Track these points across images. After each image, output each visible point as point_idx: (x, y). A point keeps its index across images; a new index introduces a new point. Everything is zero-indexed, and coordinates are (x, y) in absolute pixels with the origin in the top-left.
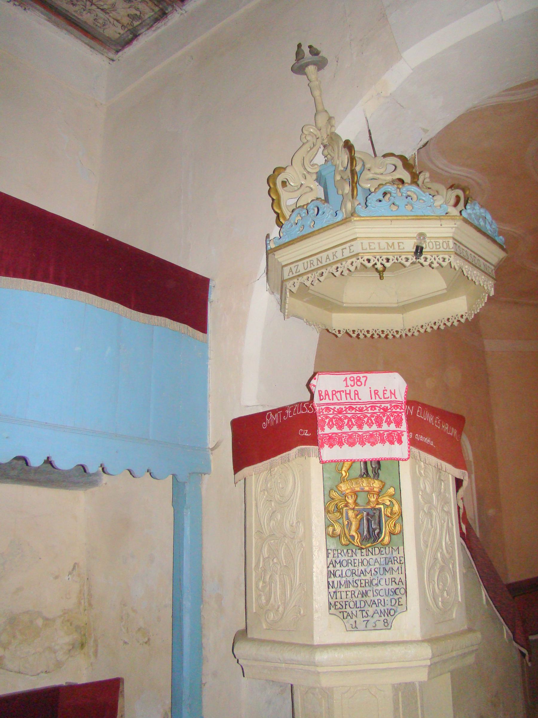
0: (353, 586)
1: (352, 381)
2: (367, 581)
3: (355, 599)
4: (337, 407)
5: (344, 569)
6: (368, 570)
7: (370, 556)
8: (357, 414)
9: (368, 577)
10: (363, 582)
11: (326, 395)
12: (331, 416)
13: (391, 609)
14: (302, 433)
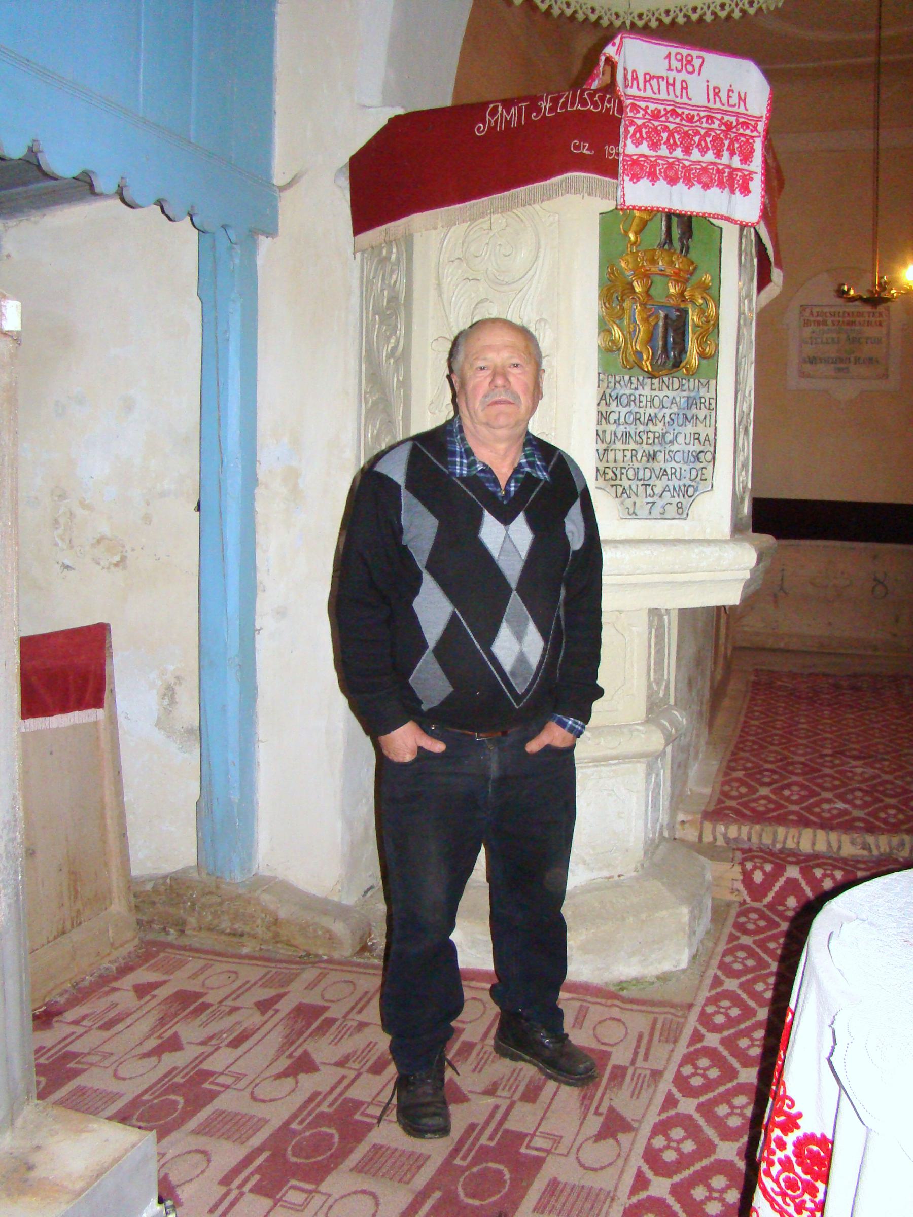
0: (636, 442)
1: (678, 61)
2: (657, 434)
3: (636, 465)
4: (652, 107)
5: (624, 411)
6: (660, 416)
7: (666, 392)
8: (681, 127)
9: (659, 428)
10: (651, 435)
11: (633, 79)
12: (639, 122)
13: (690, 486)
14: (577, 147)
